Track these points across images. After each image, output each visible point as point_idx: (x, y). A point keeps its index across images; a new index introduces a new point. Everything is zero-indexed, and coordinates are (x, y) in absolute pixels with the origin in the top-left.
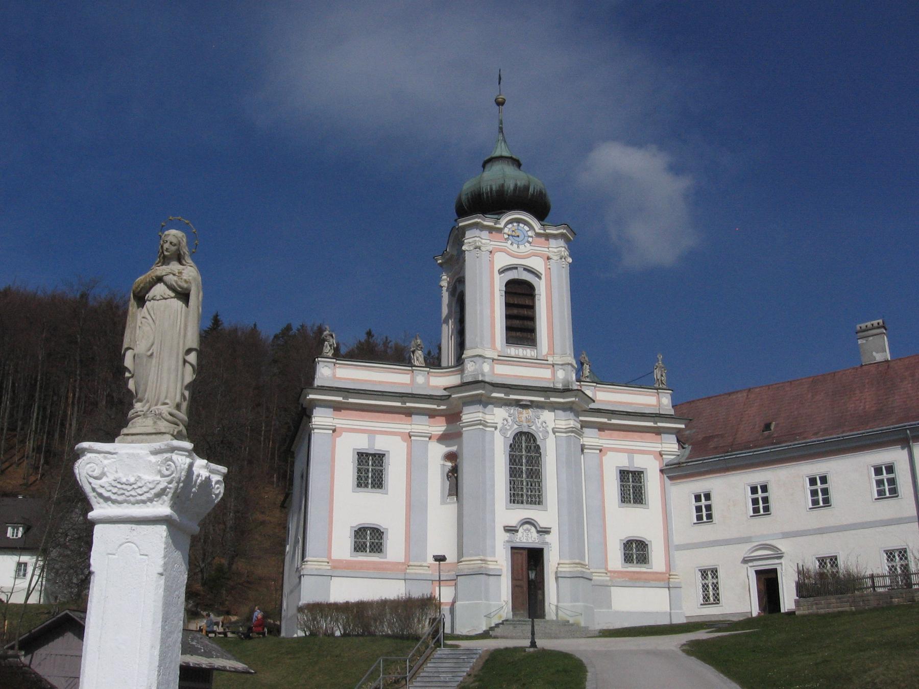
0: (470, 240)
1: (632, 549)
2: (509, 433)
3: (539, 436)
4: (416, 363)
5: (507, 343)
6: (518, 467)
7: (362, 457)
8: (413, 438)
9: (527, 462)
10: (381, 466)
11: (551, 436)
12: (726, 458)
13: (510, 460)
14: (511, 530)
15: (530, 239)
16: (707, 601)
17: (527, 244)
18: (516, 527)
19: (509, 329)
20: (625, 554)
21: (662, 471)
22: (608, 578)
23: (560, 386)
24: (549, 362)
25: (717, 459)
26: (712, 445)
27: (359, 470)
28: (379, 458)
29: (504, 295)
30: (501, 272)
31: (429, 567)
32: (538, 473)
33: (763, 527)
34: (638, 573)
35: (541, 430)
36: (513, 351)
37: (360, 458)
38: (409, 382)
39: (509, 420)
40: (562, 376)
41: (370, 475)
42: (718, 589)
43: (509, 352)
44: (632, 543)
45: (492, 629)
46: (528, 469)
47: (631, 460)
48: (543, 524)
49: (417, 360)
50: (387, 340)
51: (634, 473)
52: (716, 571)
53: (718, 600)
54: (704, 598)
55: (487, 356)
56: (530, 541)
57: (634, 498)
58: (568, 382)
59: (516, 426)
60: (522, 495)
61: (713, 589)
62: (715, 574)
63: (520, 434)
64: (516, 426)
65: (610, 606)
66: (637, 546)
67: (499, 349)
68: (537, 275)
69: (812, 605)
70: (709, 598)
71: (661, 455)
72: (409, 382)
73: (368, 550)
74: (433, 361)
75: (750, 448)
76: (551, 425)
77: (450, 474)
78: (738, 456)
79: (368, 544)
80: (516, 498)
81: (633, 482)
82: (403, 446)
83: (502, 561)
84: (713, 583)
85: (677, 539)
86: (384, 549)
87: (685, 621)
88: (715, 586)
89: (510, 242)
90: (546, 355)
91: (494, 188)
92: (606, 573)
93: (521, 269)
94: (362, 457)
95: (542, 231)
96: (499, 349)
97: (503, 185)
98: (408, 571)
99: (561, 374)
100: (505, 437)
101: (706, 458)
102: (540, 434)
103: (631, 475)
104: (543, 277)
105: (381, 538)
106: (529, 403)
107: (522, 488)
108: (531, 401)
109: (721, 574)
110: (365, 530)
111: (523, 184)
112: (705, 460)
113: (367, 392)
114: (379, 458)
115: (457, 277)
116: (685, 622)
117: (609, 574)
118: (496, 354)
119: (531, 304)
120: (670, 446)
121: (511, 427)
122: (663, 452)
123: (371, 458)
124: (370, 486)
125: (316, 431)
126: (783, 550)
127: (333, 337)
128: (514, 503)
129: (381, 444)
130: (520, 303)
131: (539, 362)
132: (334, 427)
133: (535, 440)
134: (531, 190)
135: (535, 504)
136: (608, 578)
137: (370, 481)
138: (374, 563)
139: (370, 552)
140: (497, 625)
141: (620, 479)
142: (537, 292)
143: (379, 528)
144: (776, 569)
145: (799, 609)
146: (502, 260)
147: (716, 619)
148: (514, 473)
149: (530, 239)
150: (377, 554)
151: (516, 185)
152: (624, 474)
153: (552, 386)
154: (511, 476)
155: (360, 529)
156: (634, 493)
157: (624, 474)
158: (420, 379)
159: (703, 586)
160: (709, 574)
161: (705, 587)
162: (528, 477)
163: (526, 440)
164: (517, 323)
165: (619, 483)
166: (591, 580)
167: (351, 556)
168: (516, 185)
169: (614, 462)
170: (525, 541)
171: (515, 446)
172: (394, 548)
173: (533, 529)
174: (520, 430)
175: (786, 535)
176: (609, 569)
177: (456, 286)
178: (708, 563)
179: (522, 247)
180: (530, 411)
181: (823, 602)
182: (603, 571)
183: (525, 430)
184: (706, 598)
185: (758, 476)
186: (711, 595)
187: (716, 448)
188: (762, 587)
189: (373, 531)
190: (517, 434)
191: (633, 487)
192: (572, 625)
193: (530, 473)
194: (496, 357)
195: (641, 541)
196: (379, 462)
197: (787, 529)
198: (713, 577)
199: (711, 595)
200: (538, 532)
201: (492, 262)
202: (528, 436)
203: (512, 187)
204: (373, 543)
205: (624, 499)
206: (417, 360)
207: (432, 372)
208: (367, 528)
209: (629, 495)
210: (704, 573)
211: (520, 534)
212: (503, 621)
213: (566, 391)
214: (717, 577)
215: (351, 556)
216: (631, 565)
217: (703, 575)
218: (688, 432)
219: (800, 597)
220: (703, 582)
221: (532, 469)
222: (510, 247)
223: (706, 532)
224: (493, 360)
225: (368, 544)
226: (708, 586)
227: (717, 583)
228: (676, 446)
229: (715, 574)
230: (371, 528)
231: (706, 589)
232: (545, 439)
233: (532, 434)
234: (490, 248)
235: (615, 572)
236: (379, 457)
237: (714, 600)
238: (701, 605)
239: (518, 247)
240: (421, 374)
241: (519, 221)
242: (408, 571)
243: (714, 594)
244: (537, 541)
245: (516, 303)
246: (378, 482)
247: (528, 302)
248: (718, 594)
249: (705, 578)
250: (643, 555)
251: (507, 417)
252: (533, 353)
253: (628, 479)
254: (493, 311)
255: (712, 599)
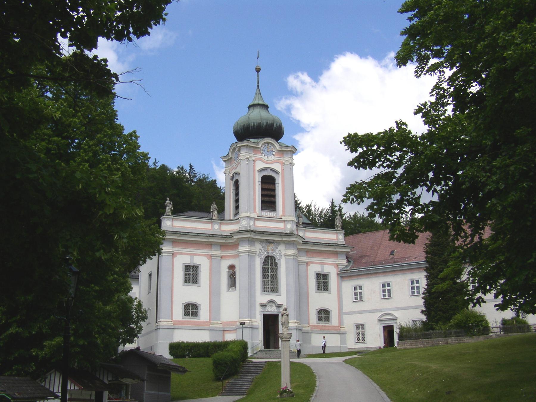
0: (243, 154)
1: (322, 314)
2: (263, 256)
3: (277, 258)
4: (214, 218)
5: (262, 209)
6: (266, 273)
7: (187, 268)
8: (212, 258)
9: (271, 271)
10: (197, 272)
11: (283, 258)
12: (370, 269)
13: (263, 271)
14: (263, 306)
15: (274, 153)
16: (359, 341)
17: (272, 156)
18: (265, 304)
19: (263, 202)
20: (318, 317)
21: (338, 274)
22: (310, 329)
23: (288, 232)
24: (283, 220)
25: (366, 269)
26: (364, 261)
27: (186, 274)
28: (195, 268)
29: (260, 184)
30: (261, 171)
31: (221, 323)
32: (277, 277)
33: (387, 304)
34: (324, 326)
35: (278, 255)
36: (265, 214)
37: (186, 268)
38: (210, 228)
39: (263, 249)
40: (290, 227)
41: (191, 277)
42: (364, 335)
43: (262, 214)
44: (322, 311)
45: (254, 354)
46: (271, 275)
47: (322, 268)
48: (279, 302)
49: (215, 216)
50: (156, 161)
51: (324, 275)
52: (364, 326)
53: (364, 340)
54: (358, 339)
55: (252, 217)
56: (272, 311)
57: (323, 288)
58: (293, 230)
59: (266, 253)
60: (269, 288)
61: (362, 335)
62: (363, 327)
63: (267, 257)
64: (266, 253)
65: (310, 343)
66: (324, 313)
67: (258, 213)
68: (277, 172)
69: (404, 344)
70: (360, 339)
71: (338, 266)
72: (210, 228)
73: (191, 315)
74: (221, 217)
75: (383, 264)
76: (283, 252)
77: (231, 276)
78: (376, 268)
79: (191, 312)
80: (265, 289)
81: (323, 280)
82: (208, 261)
83: (259, 322)
84: (362, 332)
85: (345, 309)
86: (199, 314)
87: (348, 351)
88: (363, 333)
89: (263, 155)
90: (281, 216)
91: (255, 125)
92: (309, 326)
93: (269, 170)
94: (187, 268)
95: (280, 149)
96: (258, 213)
97: (260, 123)
98: (210, 326)
99: (289, 226)
100: (261, 259)
101: (360, 268)
102: (278, 257)
103: (322, 276)
104: (280, 173)
105: (197, 309)
106: (273, 241)
107: (269, 284)
108: (274, 240)
109: (366, 327)
110: (189, 305)
111: (270, 123)
112: (360, 269)
113: (187, 234)
114: (195, 268)
115: (234, 171)
116: (348, 351)
117: (310, 327)
118: (256, 215)
119: (274, 188)
120: (343, 261)
121: (264, 253)
122: (338, 264)
123: (191, 268)
124: (191, 282)
125: (164, 254)
126: (397, 316)
127: (171, 204)
128: (265, 292)
129: (197, 260)
130: (268, 188)
131: (278, 220)
132: (173, 252)
133: (275, 260)
134: (275, 126)
135: (275, 292)
136: (310, 329)
137: (191, 280)
138: (194, 322)
139: (192, 316)
140: (257, 353)
141: (317, 278)
142: (277, 182)
143: (196, 304)
144: (393, 325)
145: (398, 346)
146: (260, 165)
147: (363, 350)
148: (265, 276)
149: (274, 153)
150: (195, 317)
151: (267, 123)
152: (318, 276)
153: (284, 232)
154: (263, 278)
155: (187, 305)
156: (323, 285)
157: (318, 276)
158: (216, 227)
159: (357, 333)
160: (360, 327)
161: (358, 334)
162: (271, 279)
163: (271, 260)
164: (267, 199)
165: (316, 280)
166: (302, 330)
167: (183, 319)
168: (267, 123)
169: (314, 269)
170: (270, 311)
171: (265, 263)
172: (204, 314)
173: (274, 305)
174: (268, 255)
175: (398, 309)
176: (310, 324)
177: (234, 176)
178: (360, 321)
179: (270, 157)
180: (273, 245)
181: (409, 343)
182: (307, 325)
183: (270, 255)
184: (358, 339)
185: (386, 279)
186: (361, 338)
187: (366, 263)
188: (386, 335)
189: (193, 306)
190: (266, 257)
191: (323, 282)
192: (293, 352)
193: (273, 276)
194: (257, 217)
195: (326, 310)
196: (195, 270)
197: (399, 305)
198: (362, 329)
199: (361, 338)
200: (277, 306)
201: (254, 166)
202: (272, 258)
203: (265, 124)
204: (193, 311)
205: (319, 288)
206: (215, 216)
207: (222, 223)
208: (190, 304)
209: (321, 286)
210: (357, 326)
211: (267, 308)
212: (260, 350)
213: (291, 235)
214: (364, 329)
215: (183, 319)
216: (321, 322)
217: (357, 328)
218: (352, 253)
219: (399, 340)
220: (357, 331)
221: (273, 275)
222: (264, 158)
223: (359, 306)
224: (255, 219)
225: (191, 312)
226: (359, 333)
227: (364, 332)
228: (346, 261)
229: (363, 327)
230: (192, 304)
231: (358, 335)
232: (280, 260)
233: (273, 257)
234: (254, 158)
235: (313, 326)
236: (196, 267)
237: (362, 341)
238: (356, 343)
239: (268, 158)
240: (216, 224)
241: (268, 143)
242: (210, 326)
243: (362, 338)
244: (276, 311)
245: (266, 188)
246: (195, 281)
247: (271, 187)
248: (364, 337)
249: (358, 329)
250: (327, 317)
251: (261, 248)
252: (274, 214)
253: (321, 278)
254: (254, 193)
255: (361, 340)
